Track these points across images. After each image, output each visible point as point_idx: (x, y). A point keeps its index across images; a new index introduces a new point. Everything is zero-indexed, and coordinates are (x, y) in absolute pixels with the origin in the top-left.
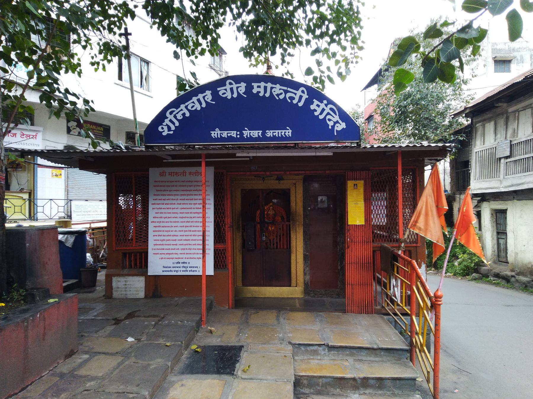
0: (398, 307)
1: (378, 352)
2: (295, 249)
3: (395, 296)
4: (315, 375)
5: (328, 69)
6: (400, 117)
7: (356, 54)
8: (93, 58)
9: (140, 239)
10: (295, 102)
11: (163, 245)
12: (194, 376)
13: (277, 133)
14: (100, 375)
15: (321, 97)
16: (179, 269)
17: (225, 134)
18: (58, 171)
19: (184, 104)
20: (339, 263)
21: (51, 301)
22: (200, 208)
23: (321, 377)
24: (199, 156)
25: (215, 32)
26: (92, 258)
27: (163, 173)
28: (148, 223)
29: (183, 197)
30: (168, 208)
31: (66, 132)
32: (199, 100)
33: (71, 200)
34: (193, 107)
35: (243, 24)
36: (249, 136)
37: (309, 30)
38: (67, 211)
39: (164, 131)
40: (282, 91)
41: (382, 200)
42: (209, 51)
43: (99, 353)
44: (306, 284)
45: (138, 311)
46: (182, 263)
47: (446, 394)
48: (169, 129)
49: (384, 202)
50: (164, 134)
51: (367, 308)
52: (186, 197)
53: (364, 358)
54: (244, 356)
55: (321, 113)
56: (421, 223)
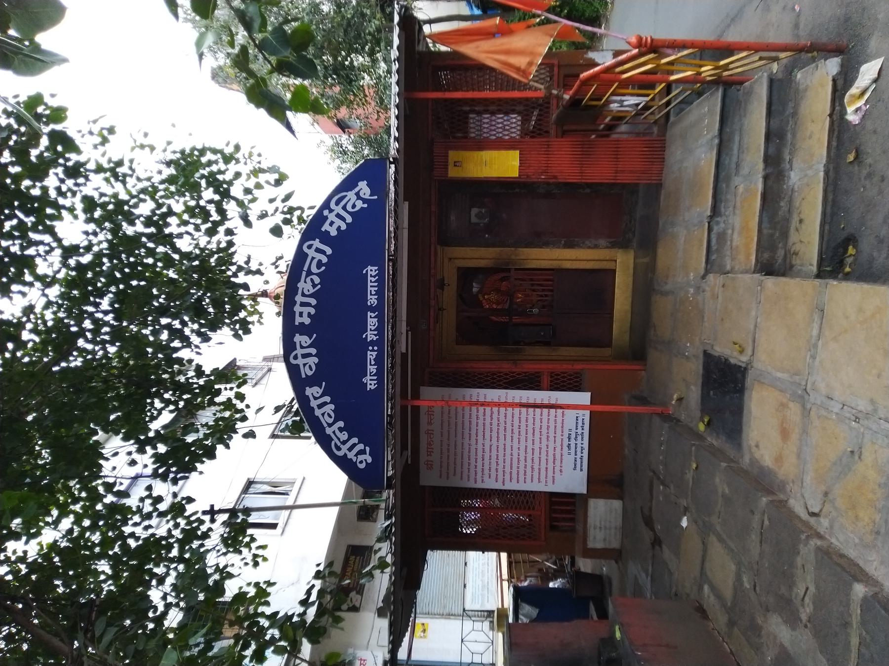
0: (657, 97)
1: (725, 137)
2: (555, 262)
3: (638, 105)
4: (755, 239)
5: (272, 201)
6: (343, 77)
7: (247, 157)
8: (246, 564)
9: (529, 503)
10: (325, 260)
11: (539, 469)
12: (745, 428)
13: (372, 288)
14: (733, 567)
15: (320, 218)
16: (579, 446)
17: (372, 369)
18: (419, 629)
19: (324, 428)
20: (581, 191)
21: (618, 635)
22: (485, 410)
23: (760, 231)
24: (404, 409)
25: (208, 376)
26: (556, 579)
27: (427, 464)
28: (505, 490)
29: (466, 436)
30: (483, 460)
31: (357, 614)
32: (320, 406)
33: (464, 610)
34: (330, 416)
35: (199, 334)
36: (376, 332)
37: (211, 232)
38: (481, 617)
39: (366, 460)
40: (308, 280)
41: (481, 121)
42: (239, 386)
43: (702, 568)
44: (613, 245)
45: (642, 511)
46: (569, 441)
47: (802, 26)
48: (362, 452)
49: (485, 118)
50: (370, 460)
51: (655, 149)
52: (467, 431)
53: (734, 159)
54: (721, 349)
55: (343, 219)
56: (521, 61)
